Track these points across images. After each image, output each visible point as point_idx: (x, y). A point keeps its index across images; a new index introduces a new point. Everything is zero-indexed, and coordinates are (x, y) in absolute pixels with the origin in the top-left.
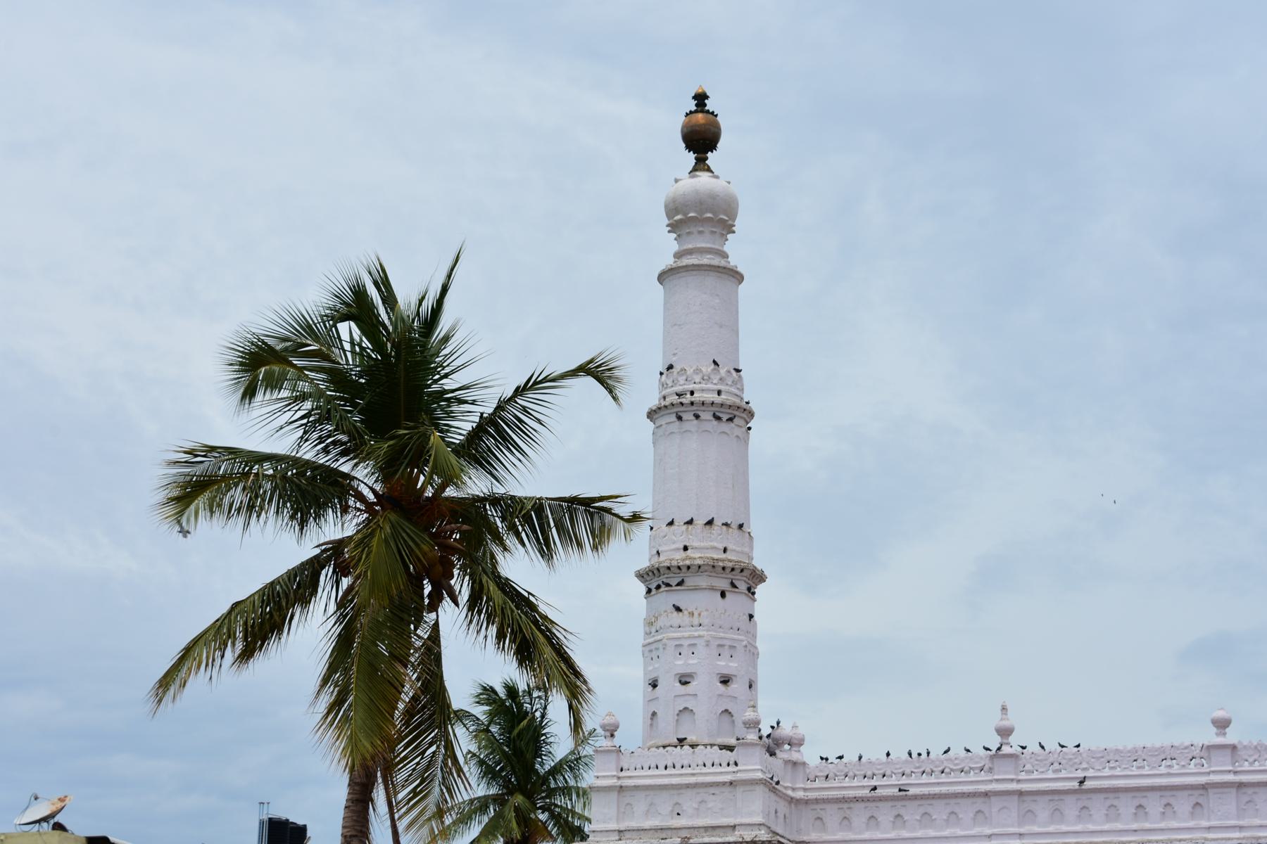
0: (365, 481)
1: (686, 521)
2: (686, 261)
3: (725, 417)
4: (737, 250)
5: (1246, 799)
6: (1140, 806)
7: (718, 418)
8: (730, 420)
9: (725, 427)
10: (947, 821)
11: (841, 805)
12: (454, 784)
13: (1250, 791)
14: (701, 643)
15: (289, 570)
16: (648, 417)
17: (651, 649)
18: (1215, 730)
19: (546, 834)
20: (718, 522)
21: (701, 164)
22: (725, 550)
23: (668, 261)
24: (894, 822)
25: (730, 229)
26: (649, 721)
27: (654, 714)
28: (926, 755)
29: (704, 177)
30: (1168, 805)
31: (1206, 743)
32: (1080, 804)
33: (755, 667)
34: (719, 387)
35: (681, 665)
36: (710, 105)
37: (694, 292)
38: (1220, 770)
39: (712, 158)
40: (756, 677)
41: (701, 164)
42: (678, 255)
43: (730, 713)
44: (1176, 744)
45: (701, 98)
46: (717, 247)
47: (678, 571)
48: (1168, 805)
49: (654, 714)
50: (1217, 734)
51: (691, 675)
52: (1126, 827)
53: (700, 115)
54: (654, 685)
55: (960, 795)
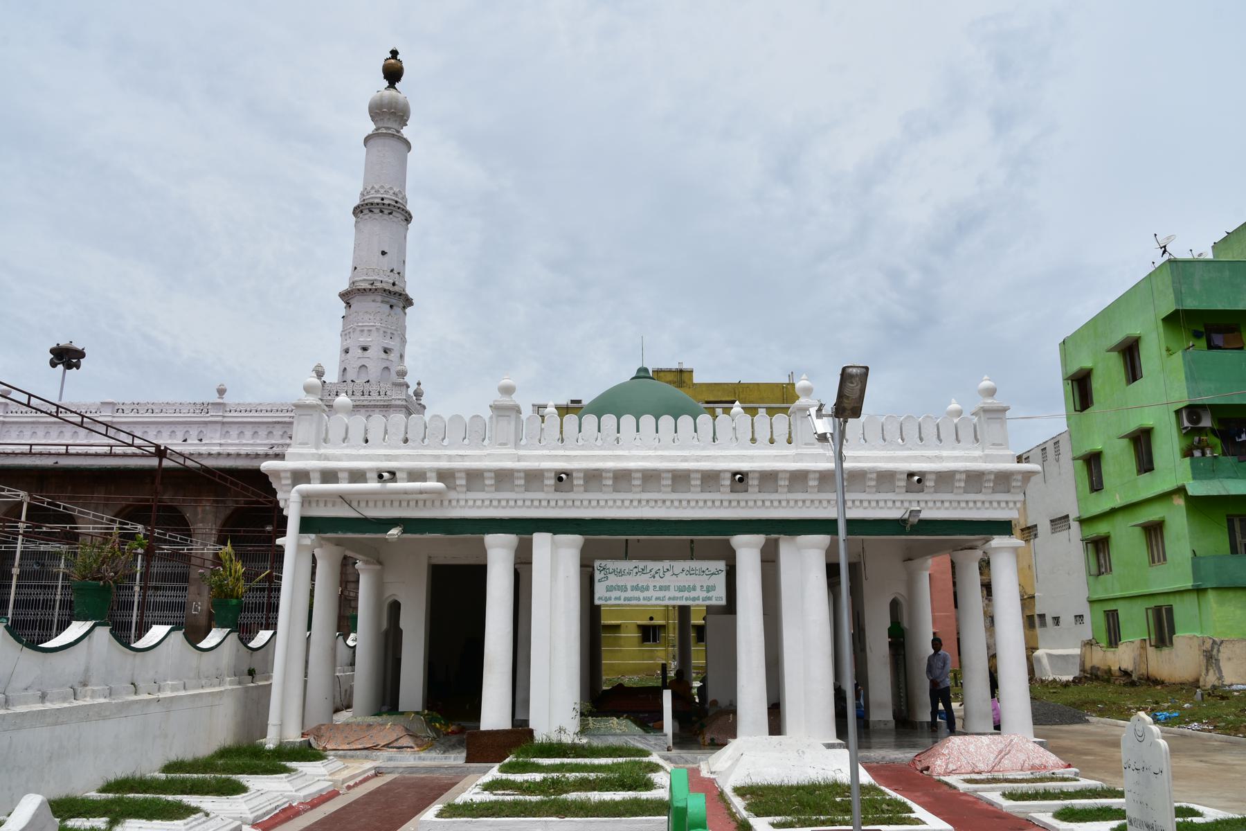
5: (6, 430)
6: (62, 432)
7: (371, 211)
8: (390, 213)
9: (386, 217)
10: (156, 435)
11: (46, 426)
13: (9, 426)
14: (374, 329)
16: (354, 213)
17: (345, 334)
18: (218, 395)
22: (394, 284)
24: (170, 435)
26: (342, 373)
27: (345, 369)
29: (392, 92)
30: (21, 431)
31: (211, 402)
33: (404, 347)
34: (383, 196)
35: (364, 340)
36: (398, 57)
37: (386, 148)
38: (215, 415)
39: (397, 85)
40: (404, 353)
42: (376, 130)
44: (170, 402)
45: (394, 53)
48: (21, 431)
49: (345, 369)
50: (219, 398)
51: (390, 350)
52: (234, 442)
53: (393, 61)
54: (347, 351)
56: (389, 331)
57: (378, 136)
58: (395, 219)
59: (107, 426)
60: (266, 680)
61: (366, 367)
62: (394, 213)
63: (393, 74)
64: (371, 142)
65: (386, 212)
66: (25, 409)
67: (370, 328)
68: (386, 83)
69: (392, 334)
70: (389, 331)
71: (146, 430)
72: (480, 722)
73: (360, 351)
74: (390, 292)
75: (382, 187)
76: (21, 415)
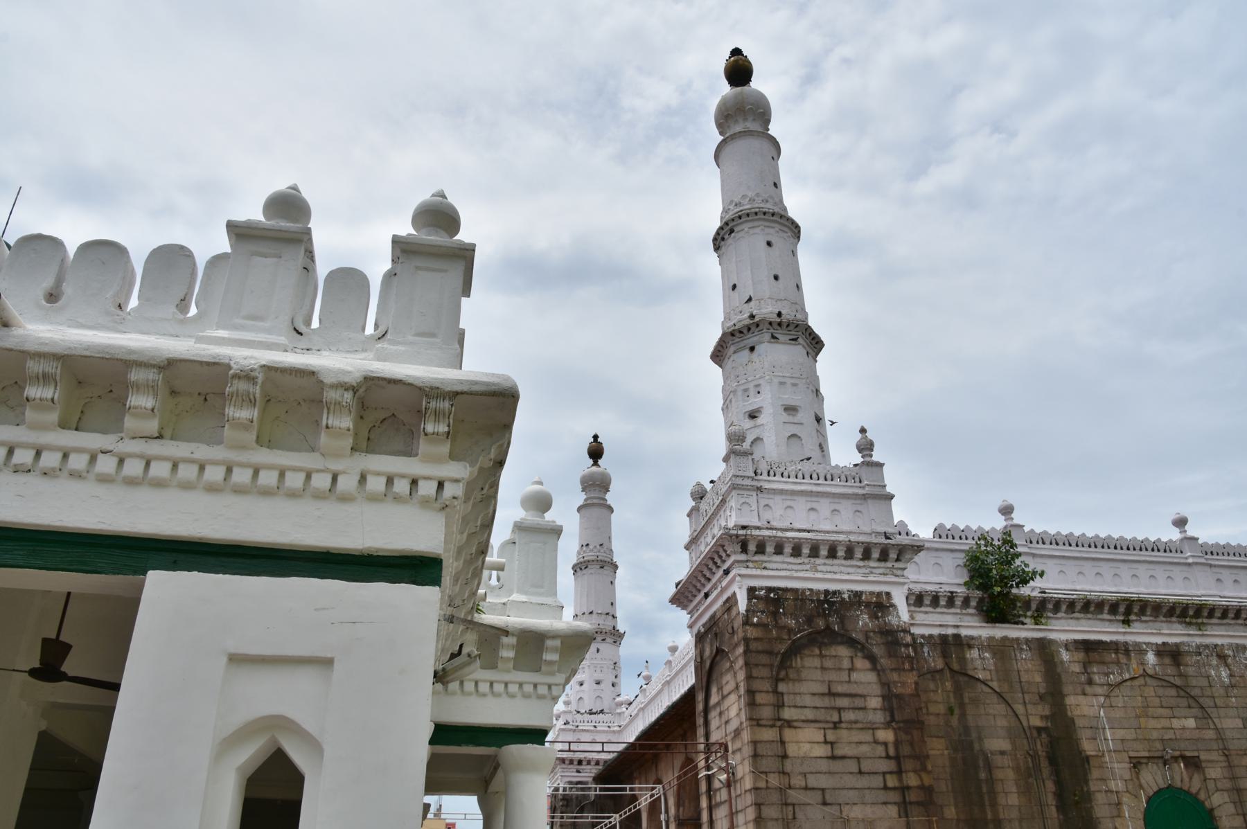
0: (1127, 676)
1: (746, 300)
2: (588, 502)
3: (583, 568)
4: (610, 498)
9: (584, 571)
12: (788, 573)
15: (1228, 544)
19: (902, 634)
20: (594, 613)
21: (596, 464)
23: (581, 502)
25: (607, 490)
28: (827, 477)
32: (809, 505)
36: (599, 440)
39: (600, 462)
41: (596, 464)
42: (586, 500)
43: (800, 437)
46: (601, 496)
47: (742, 335)
55: (821, 494)
56: (751, 386)
57: (732, 139)
58: (741, 234)
59: (860, 772)
60: (295, 220)
61: (601, 698)
62: (589, 566)
63: (596, 452)
64: (723, 156)
65: (583, 568)
66: (767, 770)
67: (602, 665)
68: (591, 462)
69: (758, 386)
70: (751, 386)
71: (814, 505)
72: (28, 791)
73: (747, 420)
74: (741, 332)
75: (758, 195)
76: (960, 541)
